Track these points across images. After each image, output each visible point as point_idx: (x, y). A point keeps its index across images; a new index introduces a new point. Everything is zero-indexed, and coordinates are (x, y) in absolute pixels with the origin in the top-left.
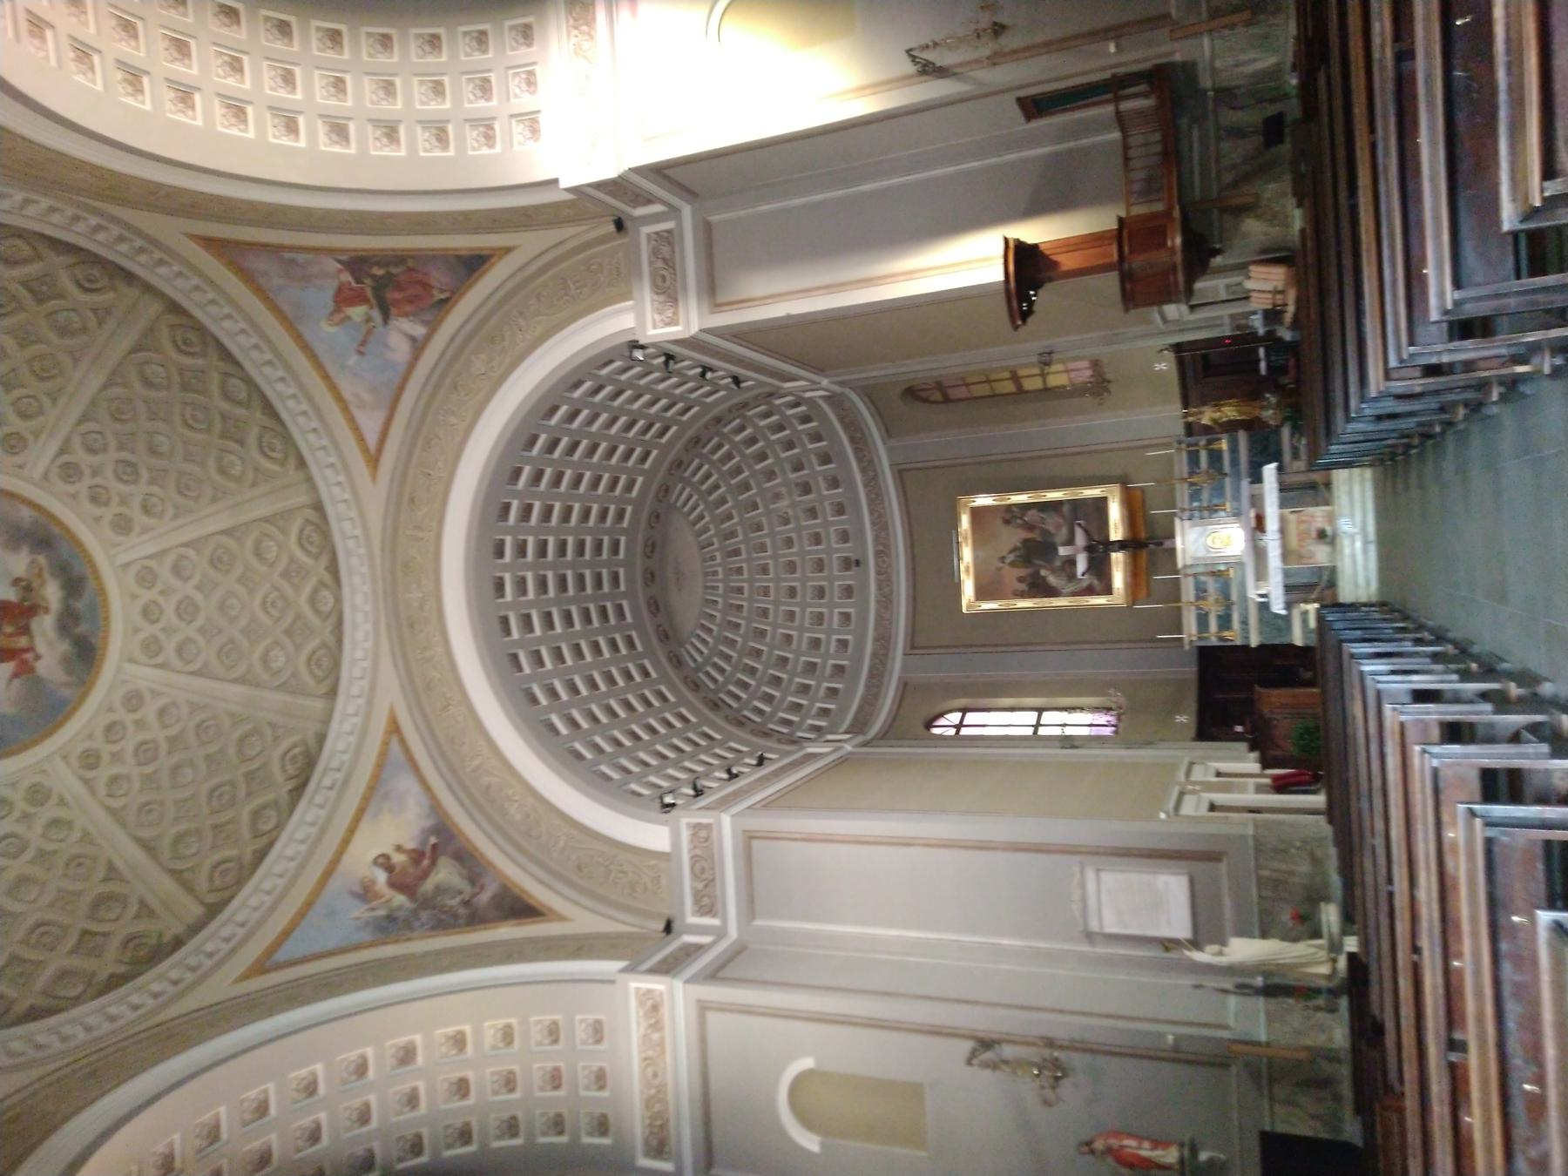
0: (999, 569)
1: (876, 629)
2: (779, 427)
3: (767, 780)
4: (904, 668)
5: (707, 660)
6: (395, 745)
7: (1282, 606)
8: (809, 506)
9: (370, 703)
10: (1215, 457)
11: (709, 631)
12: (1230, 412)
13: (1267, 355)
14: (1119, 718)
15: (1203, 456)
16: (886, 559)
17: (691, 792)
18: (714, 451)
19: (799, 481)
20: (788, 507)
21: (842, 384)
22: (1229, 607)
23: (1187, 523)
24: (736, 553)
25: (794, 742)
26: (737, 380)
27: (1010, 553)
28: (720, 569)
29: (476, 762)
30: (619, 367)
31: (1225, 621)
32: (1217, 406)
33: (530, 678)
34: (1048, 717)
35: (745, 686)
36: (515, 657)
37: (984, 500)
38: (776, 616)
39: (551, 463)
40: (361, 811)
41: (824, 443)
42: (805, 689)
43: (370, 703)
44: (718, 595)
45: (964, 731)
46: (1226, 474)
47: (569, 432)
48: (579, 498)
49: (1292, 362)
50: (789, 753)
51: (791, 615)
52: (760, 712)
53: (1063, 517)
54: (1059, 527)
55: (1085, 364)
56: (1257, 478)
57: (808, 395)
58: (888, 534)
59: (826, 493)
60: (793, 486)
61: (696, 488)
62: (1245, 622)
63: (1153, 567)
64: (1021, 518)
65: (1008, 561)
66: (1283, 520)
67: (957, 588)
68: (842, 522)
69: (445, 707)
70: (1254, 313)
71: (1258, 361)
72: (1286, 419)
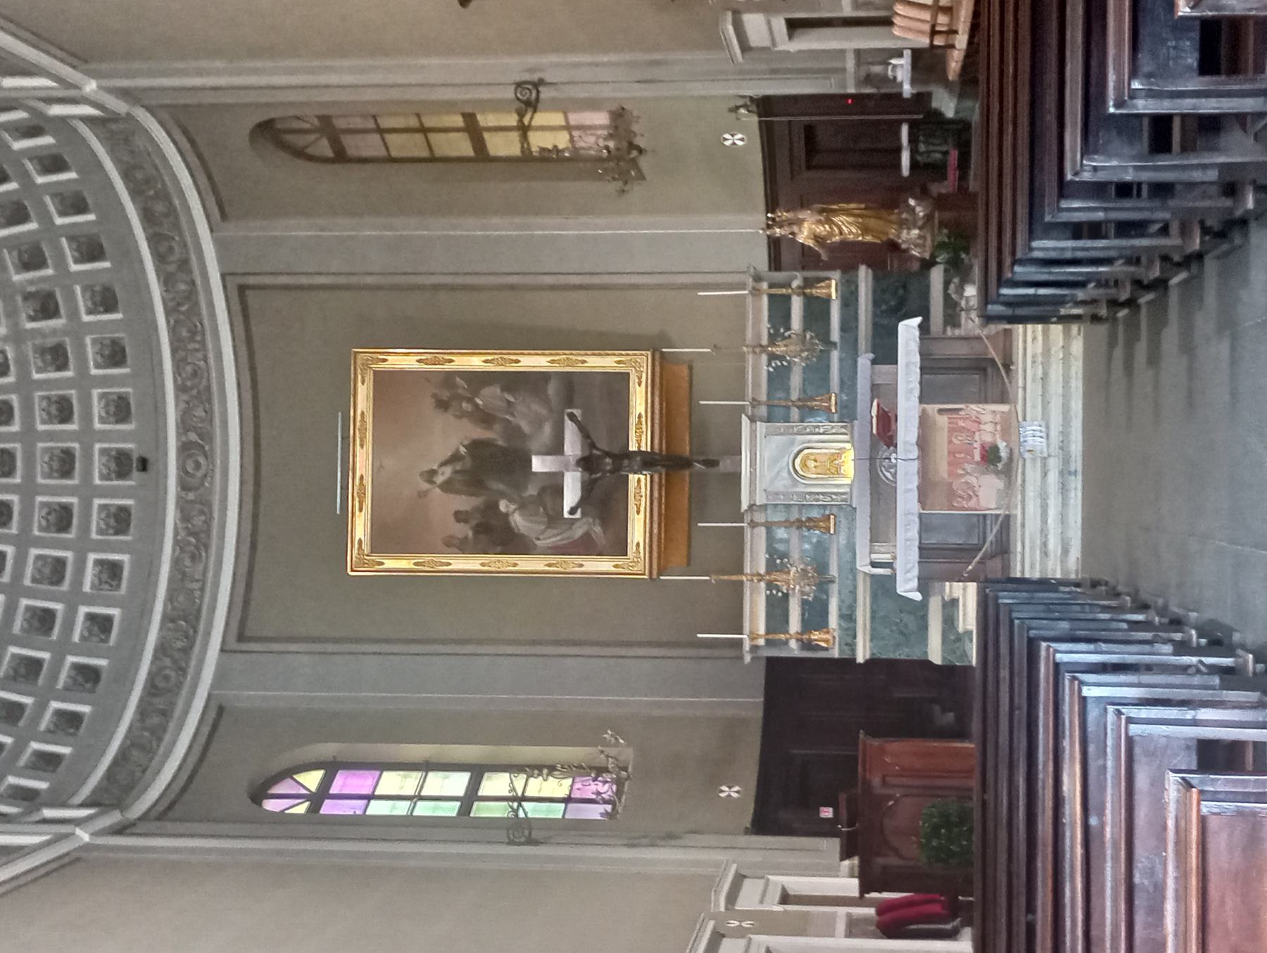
0: (423, 495)
1: (170, 598)
4: (221, 677)
7: (915, 584)
8: (51, 342)
10: (817, 311)
12: (846, 227)
13: (913, 140)
14: (619, 783)
15: (797, 304)
16: (202, 460)
19: (32, 289)
21: (124, 94)
22: (823, 584)
23: (761, 427)
27: (444, 464)
31: (815, 615)
32: (827, 215)
34: (495, 784)
37: (404, 360)
41: (91, 217)
45: (328, 808)
46: (834, 344)
49: (954, 156)
53: (546, 401)
54: (538, 423)
55: (600, 118)
56: (886, 352)
57: (57, 110)
58: (209, 412)
59: (86, 318)
60: (19, 299)
62: (848, 617)
63: (699, 508)
64: (470, 400)
65: (440, 479)
66: (924, 421)
67: (342, 525)
70: (899, 53)
71: (898, 150)
72: (941, 246)
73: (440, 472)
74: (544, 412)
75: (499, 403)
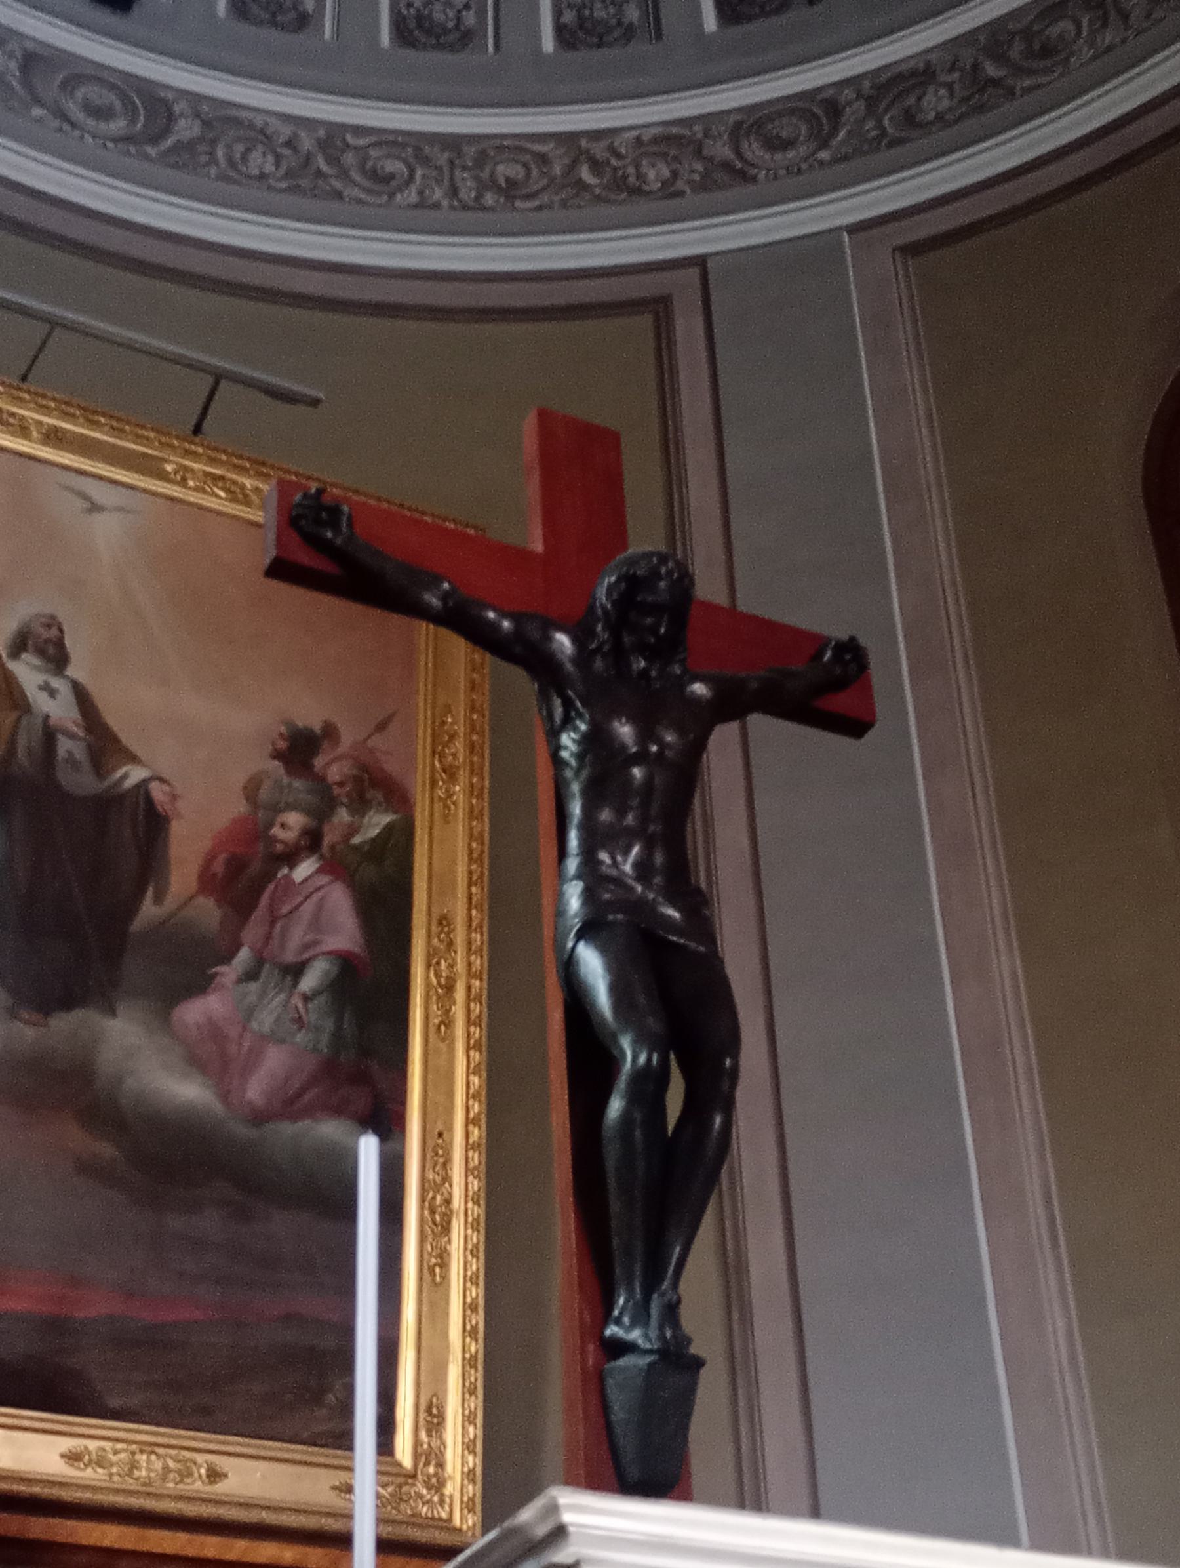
16: (118, 126)
27: (82, 696)
64: (312, 841)
73: (56, 683)
74: (255, 1091)
75: (297, 935)
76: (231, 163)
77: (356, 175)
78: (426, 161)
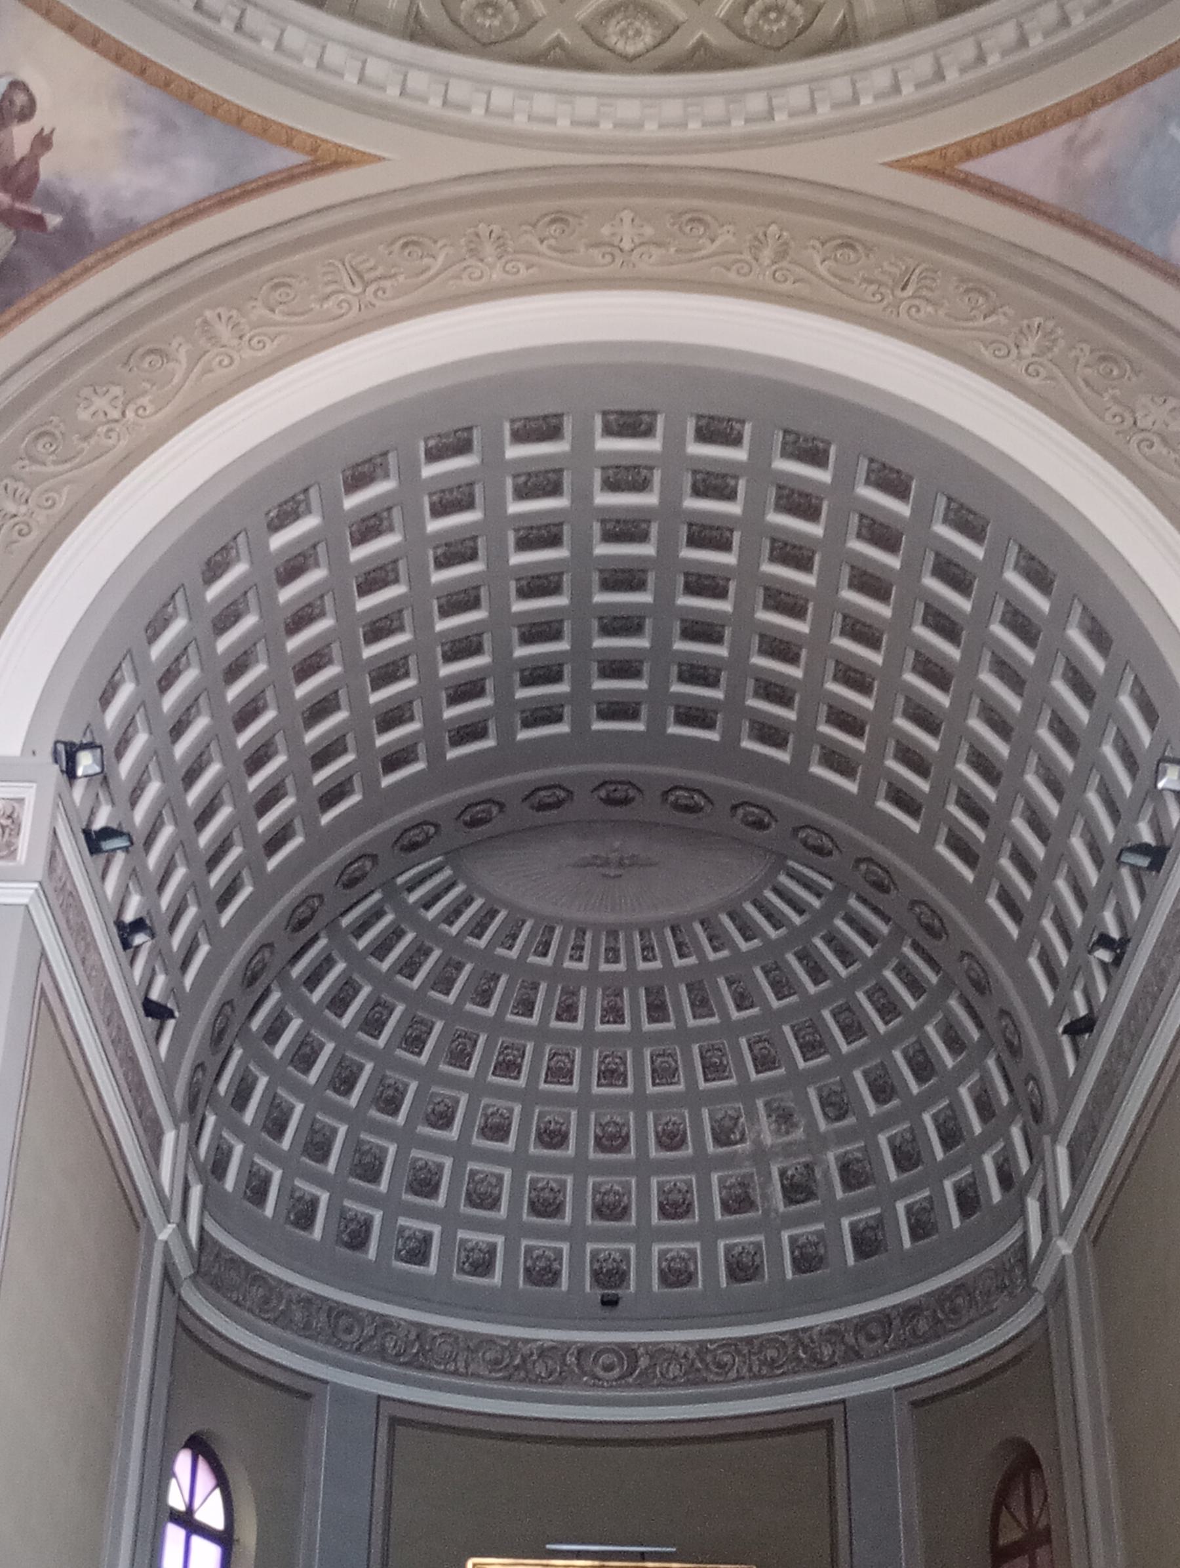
1: (447, 1333)
2: (951, 1135)
3: (111, 1018)
4: (345, 1396)
5: (408, 914)
6: (282, 159)
9: (384, 111)
11: (478, 928)
16: (616, 1372)
17: (98, 825)
18: (905, 972)
20: (758, 1143)
21: (1058, 1288)
24: (657, 1011)
25: (192, 1103)
26: (1081, 1028)
28: (621, 967)
29: (224, 331)
30: (1084, 875)
33: (409, 474)
35: (339, 1002)
36: (462, 447)
38: (500, 1092)
39: (903, 617)
40: (142, 68)
41: (907, 1243)
42: (318, 1146)
43: (384, 111)
44: (559, 959)
47: (982, 615)
48: (814, 677)
50: (168, 1095)
51: (498, 1131)
52: (273, 1033)
57: (1033, 1207)
58: (673, 1383)
60: (806, 1159)
61: (820, 920)
68: (712, 1273)
69: (360, 276)
76: (662, 1374)
77: (713, 1368)
78: (739, 1352)
